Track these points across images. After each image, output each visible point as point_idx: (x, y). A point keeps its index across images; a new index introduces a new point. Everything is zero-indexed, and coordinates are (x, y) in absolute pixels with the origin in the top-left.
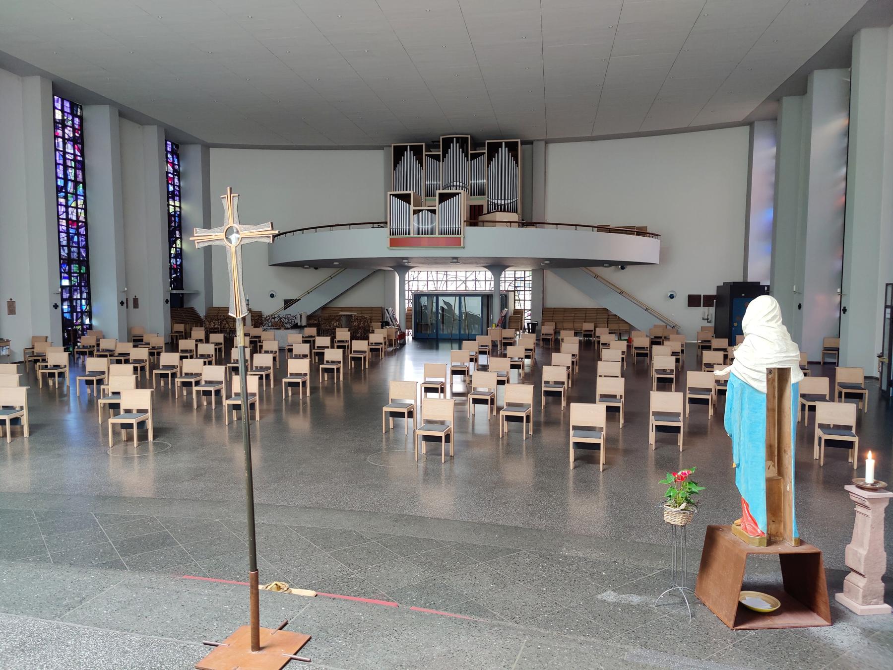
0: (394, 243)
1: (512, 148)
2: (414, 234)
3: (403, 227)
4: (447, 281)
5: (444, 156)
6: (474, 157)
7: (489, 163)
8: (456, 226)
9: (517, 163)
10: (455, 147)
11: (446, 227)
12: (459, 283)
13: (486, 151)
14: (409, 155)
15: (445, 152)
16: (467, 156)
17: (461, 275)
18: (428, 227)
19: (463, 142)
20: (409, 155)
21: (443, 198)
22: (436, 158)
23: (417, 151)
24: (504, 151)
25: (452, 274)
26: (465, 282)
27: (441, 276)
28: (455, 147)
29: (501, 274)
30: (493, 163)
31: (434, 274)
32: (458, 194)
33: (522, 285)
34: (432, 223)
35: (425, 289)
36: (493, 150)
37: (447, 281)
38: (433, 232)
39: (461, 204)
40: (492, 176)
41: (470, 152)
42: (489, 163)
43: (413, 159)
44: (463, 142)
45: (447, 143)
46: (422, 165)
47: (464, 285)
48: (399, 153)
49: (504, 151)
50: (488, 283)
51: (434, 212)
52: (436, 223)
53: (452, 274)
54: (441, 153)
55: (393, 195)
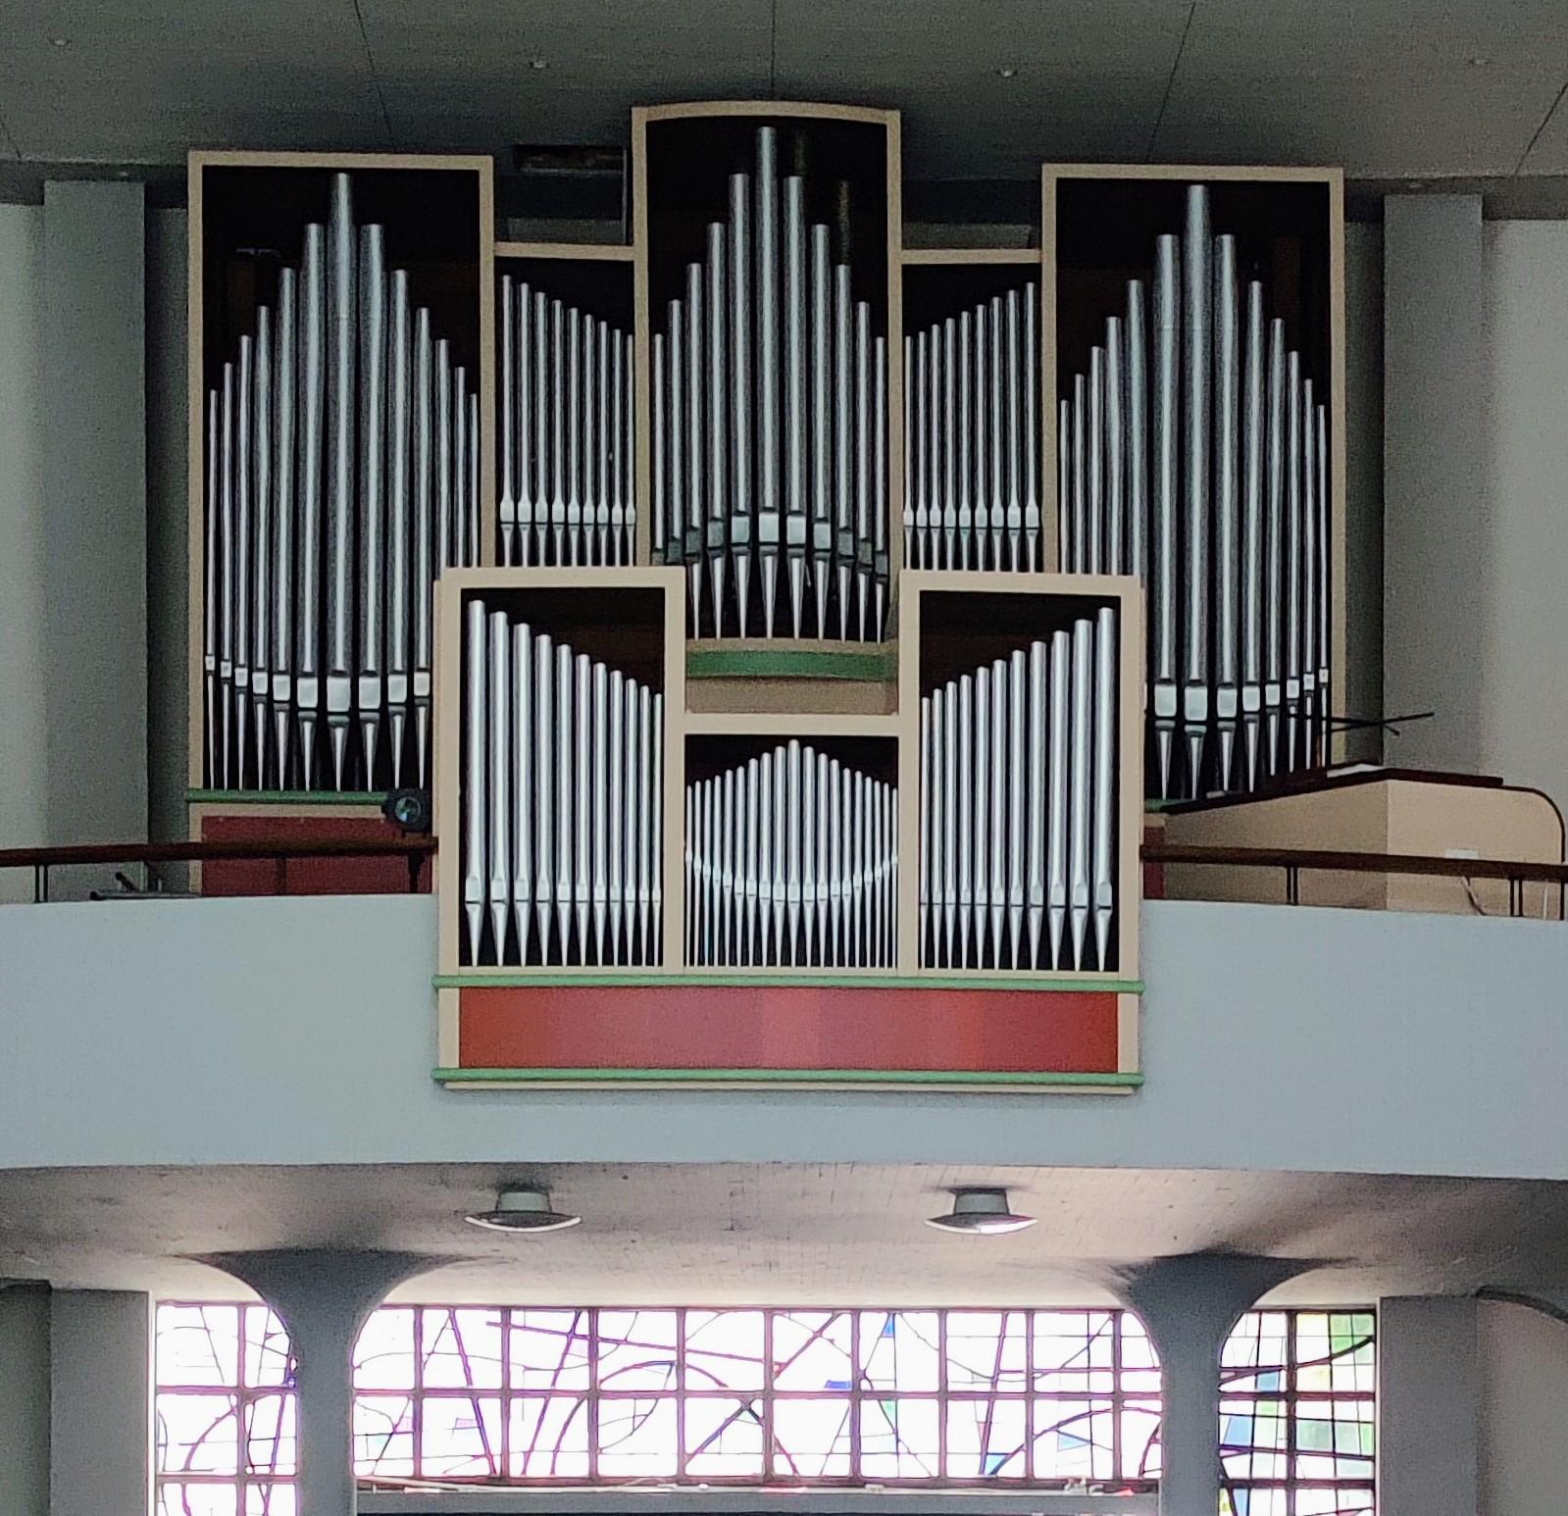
0: (497, 1038)
1: (1277, 239)
2: (696, 954)
3: (591, 892)
4: (593, 1396)
5: (668, 285)
6: (936, 298)
7: (1074, 363)
8: (1071, 888)
9: (1316, 369)
10: (766, 205)
11: (990, 897)
12: (704, 1415)
13: (1047, 257)
14: (345, 269)
15: (677, 253)
16: (869, 286)
17: (728, 1341)
18: (838, 891)
19: (835, 168)
20: (345, 269)
21: (970, 635)
22: (599, 293)
23: (426, 235)
24: (1195, 265)
25: (640, 1333)
26: (760, 1404)
27: (538, 1350)
28: (766, 205)
29: (1231, 1321)
30: (1105, 361)
31: (479, 1329)
32: (1087, 607)
33: (1270, 1433)
34: (854, 858)
35: (575, 1465)
36: (1112, 243)
37: (593, 1396)
38: (864, 936)
39: (1089, 703)
40: (1112, 466)
41: (898, 257)
42: (1074, 363)
43: (388, 294)
44: (835, 168)
45: (697, 172)
46: (465, 355)
47: (747, 1435)
48: (258, 232)
49: (1195, 265)
50: (965, 1416)
51: (875, 758)
52: (905, 860)
53: (640, 1333)
54: (638, 253)
55: (495, 599)
